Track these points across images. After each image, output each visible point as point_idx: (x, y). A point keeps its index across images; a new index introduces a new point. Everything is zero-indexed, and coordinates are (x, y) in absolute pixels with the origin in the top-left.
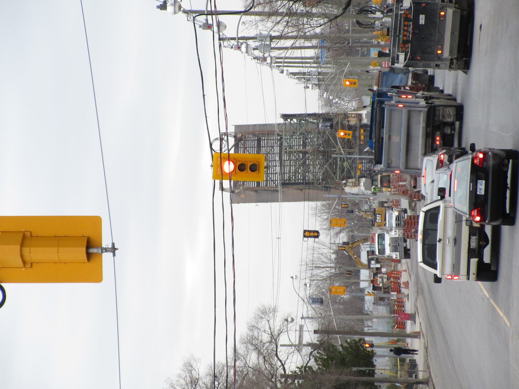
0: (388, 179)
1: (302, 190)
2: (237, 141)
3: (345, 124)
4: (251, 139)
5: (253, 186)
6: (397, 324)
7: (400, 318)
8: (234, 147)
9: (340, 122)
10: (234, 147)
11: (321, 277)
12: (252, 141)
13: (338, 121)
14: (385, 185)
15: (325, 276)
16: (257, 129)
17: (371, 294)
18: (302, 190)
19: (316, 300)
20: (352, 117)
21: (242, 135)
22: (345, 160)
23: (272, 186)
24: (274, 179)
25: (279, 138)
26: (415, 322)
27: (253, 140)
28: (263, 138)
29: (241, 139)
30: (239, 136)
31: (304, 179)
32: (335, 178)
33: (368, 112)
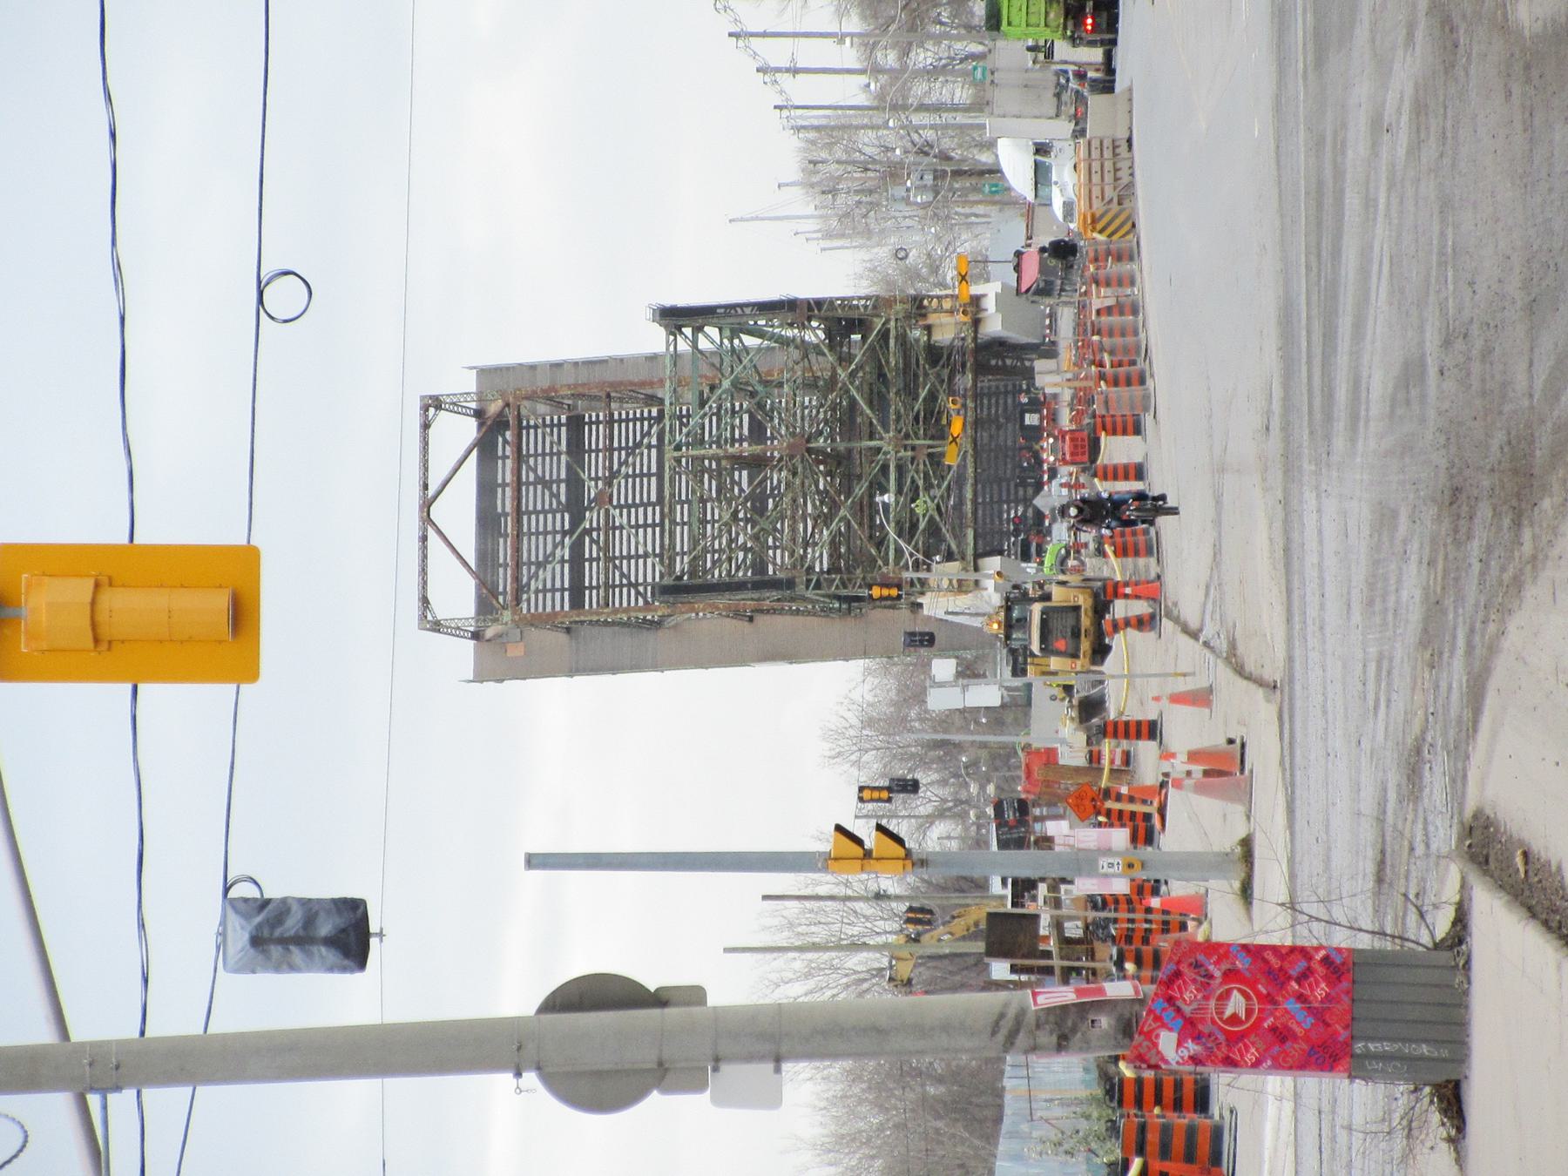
0: (1071, 621)
1: (751, 619)
2: (484, 430)
3: (917, 340)
4: (544, 419)
5: (558, 608)
6: (1141, 1151)
7: (1190, 1029)
8: (475, 452)
9: (893, 333)
10: (475, 452)
11: (846, 975)
12: (548, 430)
13: (888, 331)
14: (1061, 645)
15: (859, 968)
16: (567, 378)
17: (868, 854)
18: (751, 619)
19: (292, 924)
20: (940, 310)
21: (508, 405)
22: (918, 487)
23: (633, 604)
24: (641, 580)
25: (654, 412)
26: (1452, 1101)
27: (552, 425)
28: (590, 417)
29: (500, 424)
30: (494, 408)
31: (760, 566)
32: (880, 562)
33: (1004, 286)
